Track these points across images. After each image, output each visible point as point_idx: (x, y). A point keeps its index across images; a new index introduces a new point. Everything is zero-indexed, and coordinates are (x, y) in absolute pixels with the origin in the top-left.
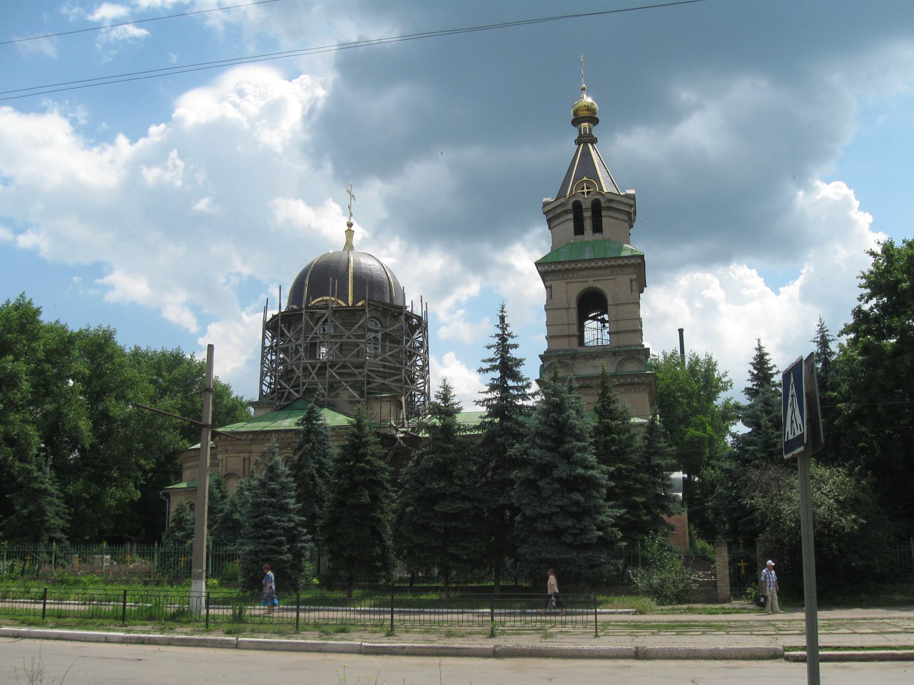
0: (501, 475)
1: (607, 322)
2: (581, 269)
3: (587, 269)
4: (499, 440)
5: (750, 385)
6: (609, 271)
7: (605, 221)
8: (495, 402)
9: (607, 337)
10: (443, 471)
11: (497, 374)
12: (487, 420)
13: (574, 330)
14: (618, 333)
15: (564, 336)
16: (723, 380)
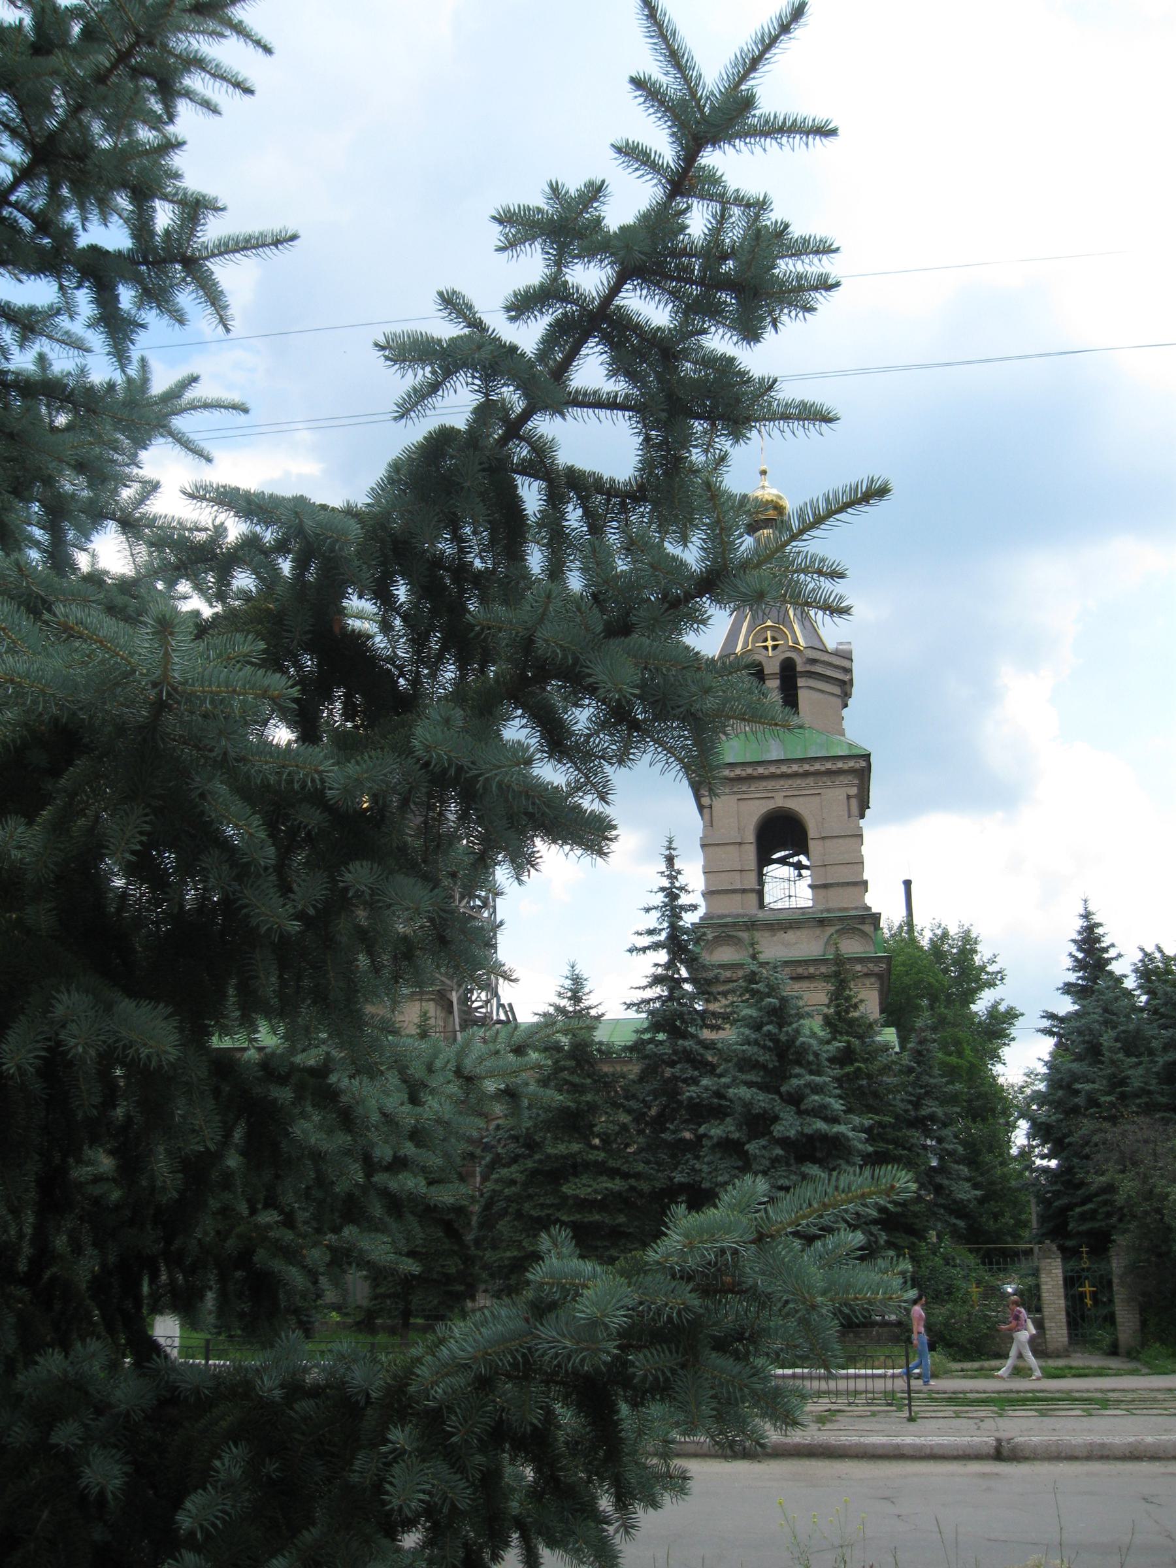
0: (674, 1132)
1: (807, 868)
2: (762, 777)
3: (773, 776)
4: (668, 1072)
5: (1072, 977)
6: (810, 781)
7: (803, 696)
8: (658, 1005)
9: (809, 893)
10: (572, 1122)
11: (663, 956)
12: (647, 1036)
13: (751, 881)
14: (826, 886)
15: (734, 891)
16: (990, 969)
